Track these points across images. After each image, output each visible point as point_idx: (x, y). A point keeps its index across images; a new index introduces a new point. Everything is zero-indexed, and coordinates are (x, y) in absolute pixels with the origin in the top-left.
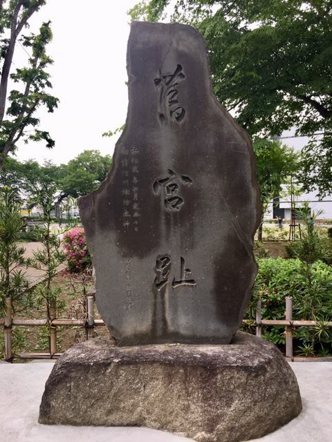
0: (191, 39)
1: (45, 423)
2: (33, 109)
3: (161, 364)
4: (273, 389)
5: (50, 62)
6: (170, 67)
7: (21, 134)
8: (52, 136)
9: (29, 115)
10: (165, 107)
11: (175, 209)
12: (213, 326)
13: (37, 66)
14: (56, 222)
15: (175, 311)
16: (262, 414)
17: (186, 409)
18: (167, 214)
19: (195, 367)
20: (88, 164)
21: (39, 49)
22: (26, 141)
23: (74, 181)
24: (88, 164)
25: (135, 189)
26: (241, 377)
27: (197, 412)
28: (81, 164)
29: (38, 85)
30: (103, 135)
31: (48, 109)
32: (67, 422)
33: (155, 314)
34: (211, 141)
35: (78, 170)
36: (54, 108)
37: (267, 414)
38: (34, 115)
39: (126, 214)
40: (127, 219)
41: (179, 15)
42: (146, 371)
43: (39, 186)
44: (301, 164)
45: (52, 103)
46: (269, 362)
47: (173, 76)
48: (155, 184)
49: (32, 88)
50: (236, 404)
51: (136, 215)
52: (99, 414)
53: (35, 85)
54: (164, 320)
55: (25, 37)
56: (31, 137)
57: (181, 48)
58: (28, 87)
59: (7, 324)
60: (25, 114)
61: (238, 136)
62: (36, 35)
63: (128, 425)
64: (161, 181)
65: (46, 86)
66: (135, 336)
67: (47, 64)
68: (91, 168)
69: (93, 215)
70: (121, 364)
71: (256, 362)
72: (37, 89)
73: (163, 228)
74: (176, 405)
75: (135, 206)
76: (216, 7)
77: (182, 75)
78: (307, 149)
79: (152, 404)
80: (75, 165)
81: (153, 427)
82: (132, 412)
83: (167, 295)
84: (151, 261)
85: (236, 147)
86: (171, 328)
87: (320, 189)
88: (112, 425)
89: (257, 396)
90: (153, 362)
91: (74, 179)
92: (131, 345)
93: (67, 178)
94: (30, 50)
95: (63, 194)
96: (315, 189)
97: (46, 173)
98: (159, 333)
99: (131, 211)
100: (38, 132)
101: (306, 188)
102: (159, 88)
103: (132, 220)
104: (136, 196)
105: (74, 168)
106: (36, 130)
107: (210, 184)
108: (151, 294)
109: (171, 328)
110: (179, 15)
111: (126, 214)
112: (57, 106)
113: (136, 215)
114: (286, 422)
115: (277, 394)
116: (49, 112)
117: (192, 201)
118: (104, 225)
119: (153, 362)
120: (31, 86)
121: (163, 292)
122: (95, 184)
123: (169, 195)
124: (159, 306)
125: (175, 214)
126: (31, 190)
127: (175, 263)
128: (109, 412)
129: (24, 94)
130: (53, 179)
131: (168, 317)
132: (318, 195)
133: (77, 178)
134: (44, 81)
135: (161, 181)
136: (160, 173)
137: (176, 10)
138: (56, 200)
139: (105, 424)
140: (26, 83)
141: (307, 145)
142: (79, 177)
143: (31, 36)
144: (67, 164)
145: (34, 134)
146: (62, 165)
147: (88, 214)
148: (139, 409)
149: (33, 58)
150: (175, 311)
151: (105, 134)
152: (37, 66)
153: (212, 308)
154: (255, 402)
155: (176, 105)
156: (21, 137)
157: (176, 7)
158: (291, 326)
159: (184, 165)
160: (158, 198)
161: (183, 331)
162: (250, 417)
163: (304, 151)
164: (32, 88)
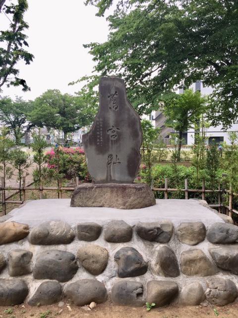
0: (120, 83)
1: (73, 207)
2: (14, 62)
3: (109, 187)
4: (144, 195)
5: (27, 27)
6: (113, 92)
7: (5, 81)
8: (28, 84)
9: (12, 66)
10: (111, 105)
11: (114, 139)
12: (127, 178)
13: (17, 29)
14: (26, 146)
15: (114, 172)
16: (140, 201)
17: (117, 200)
18: (112, 141)
19: (120, 188)
20: (51, 101)
21: (18, 17)
22: (8, 86)
23: (40, 114)
24: (51, 101)
25: (101, 132)
26: (134, 191)
27: (120, 201)
28: (45, 101)
29: (18, 44)
30: (69, 85)
31: (25, 62)
32: (80, 206)
33: (107, 174)
34: (126, 116)
35: (43, 105)
36: (30, 62)
37: (142, 202)
38: (15, 67)
39: (98, 140)
40: (98, 142)
41: (120, 10)
42: (105, 190)
43: (12, 118)
44: (208, 108)
45: (28, 58)
46: (143, 187)
47: (114, 95)
48: (108, 131)
49: (13, 46)
50: (132, 198)
51: (101, 141)
52: (90, 203)
53: (16, 45)
54: (111, 176)
55: (7, 7)
56: (12, 83)
57: (117, 86)
58: (10, 45)
59: (41, 188)
60: (8, 66)
61: (135, 115)
62: (15, 5)
63: (99, 207)
64: (110, 130)
65: (23, 45)
66: (101, 180)
67: (25, 28)
68: (53, 104)
69: (87, 140)
70: (97, 188)
71: (139, 187)
72: (16, 47)
73: (110, 145)
74: (114, 199)
75: (101, 138)
76: (146, 4)
77: (117, 95)
78: (212, 96)
79: (106, 200)
80: (41, 101)
81: (107, 207)
82: (100, 203)
83: (111, 167)
84: (106, 156)
85: (134, 119)
86: (113, 178)
87: (223, 124)
88: (94, 207)
89: (138, 196)
90: (107, 187)
91: (40, 112)
92: (99, 183)
93: (34, 113)
94: (11, 16)
95: (31, 124)
96: (220, 124)
97: (17, 108)
98: (109, 180)
99: (100, 139)
100: (17, 79)
101: (213, 124)
102: (109, 99)
103: (100, 142)
104: (101, 135)
105: (40, 104)
106: (16, 78)
107: (126, 131)
108: (106, 167)
109: (113, 178)
110: (120, 10)
111: (98, 140)
112: (32, 60)
113: (101, 141)
114: (149, 206)
115: (145, 197)
116: (26, 64)
117: (120, 136)
118: (91, 144)
119: (107, 187)
120: (12, 44)
121: (110, 166)
122: (57, 116)
123: (113, 134)
124: (109, 171)
125: (114, 140)
126: (6, 121)
127: (114, 157)
128: (93, 203)
129: (7, 50)
130: (23, 112)
131: (112, 174)
132: (223, 129)
133: (42, 112)
134: (22, 42)
135: (110, 130)
136: (109, 127)
137: (118, 8)
138: (25, 129)
139: (91, 207)
140: (8, 42)
141: (212, 93)
142: (44, 111)
143: (12, 5)
144: (34, 101)
145: (14, 80)
146: (30, 101)
147: (86, 140)
148: (102, 202)
149: (14, 23)
150: (114, 172)
151: (70, 84)
152: (17, 29)
153: (127, 172)
154: (138, 198)
155: (115, 104)
156: (5, 83)
157: (118, 6)
158: (166, 191)
159: (118, 124)
160: (109, 135)
161: (117, 179)
162: (136, 202)
163: (210, 98)
164: (13, 46)
